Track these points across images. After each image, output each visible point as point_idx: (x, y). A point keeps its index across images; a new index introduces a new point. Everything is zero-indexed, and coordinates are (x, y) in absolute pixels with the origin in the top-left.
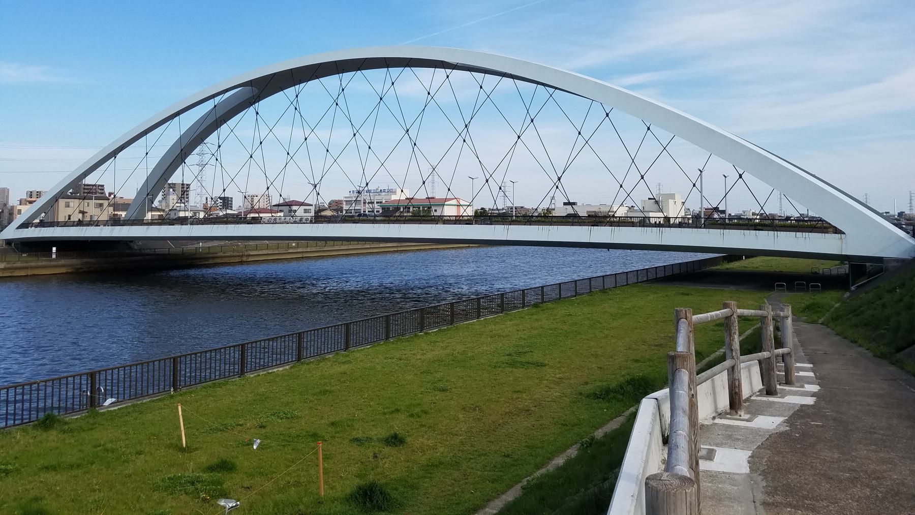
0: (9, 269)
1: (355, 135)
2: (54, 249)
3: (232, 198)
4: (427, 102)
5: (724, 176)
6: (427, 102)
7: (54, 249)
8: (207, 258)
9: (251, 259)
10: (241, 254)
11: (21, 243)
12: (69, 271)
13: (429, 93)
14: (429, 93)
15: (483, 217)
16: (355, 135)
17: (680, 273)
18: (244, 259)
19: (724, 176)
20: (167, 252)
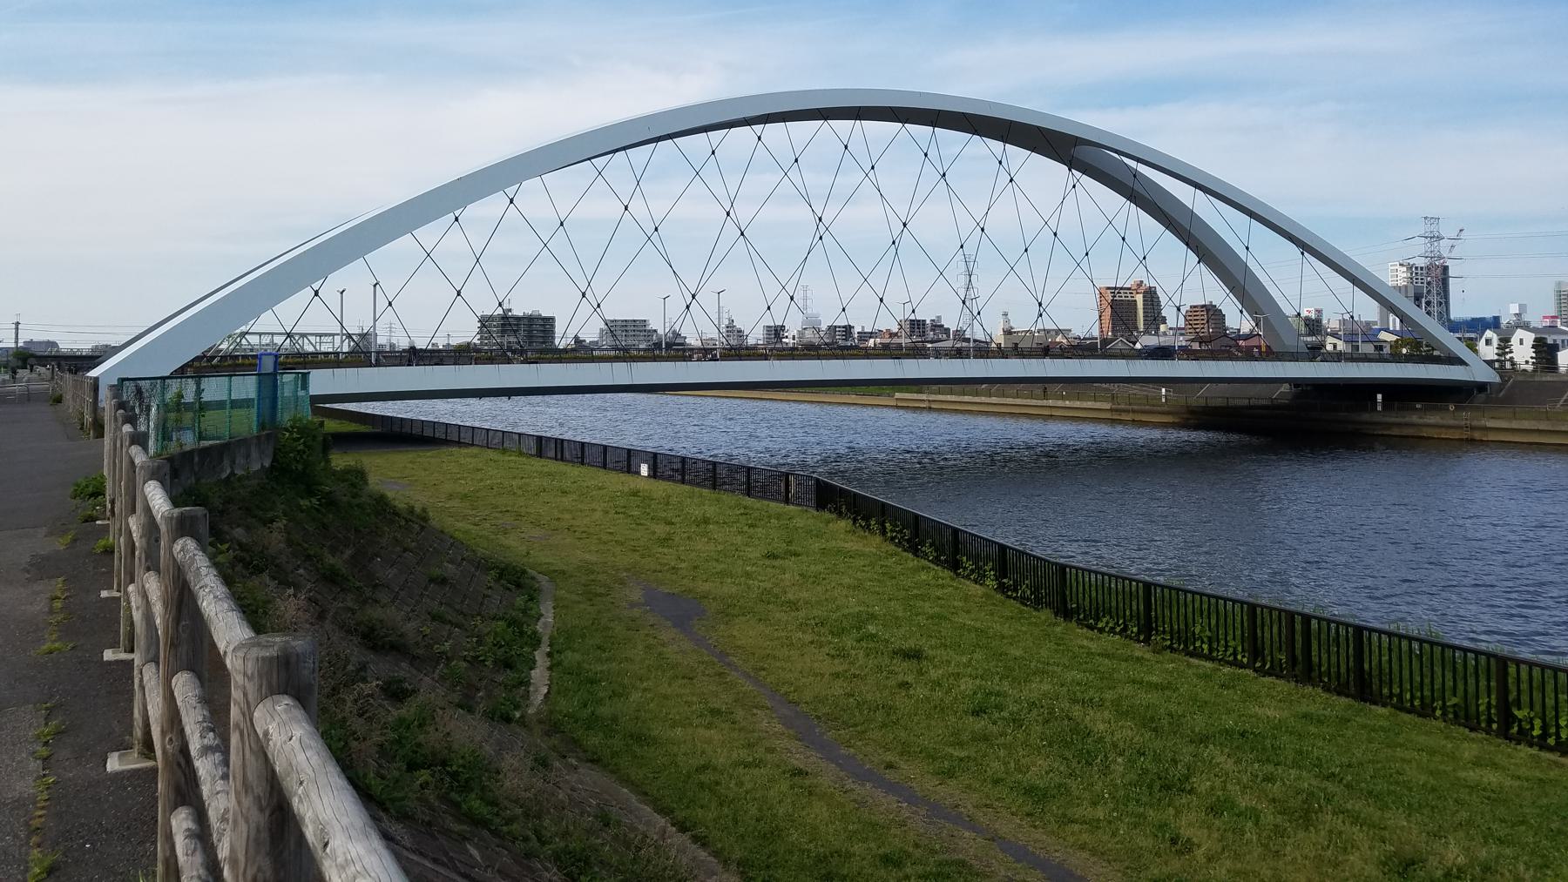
0: (1117, 410)
1: (1144, 258)
2: (1379, 397)
3: (553, 319)
4: (814, 244)
5: (343, 291)
6: (749, 246)
7: (1379, 397)
8: (1386, 423)
9: (1492, 437)
10: (1464, 422)
11: (1313, 385)
12: (1177, 421)
13: (983, 230)
14: (983, 230)
15: (1016, 348)
16: (1144, 258)
17: (411, 434)
18: (1477, 435)
19: (343, 291)
20: (1225, 404)
